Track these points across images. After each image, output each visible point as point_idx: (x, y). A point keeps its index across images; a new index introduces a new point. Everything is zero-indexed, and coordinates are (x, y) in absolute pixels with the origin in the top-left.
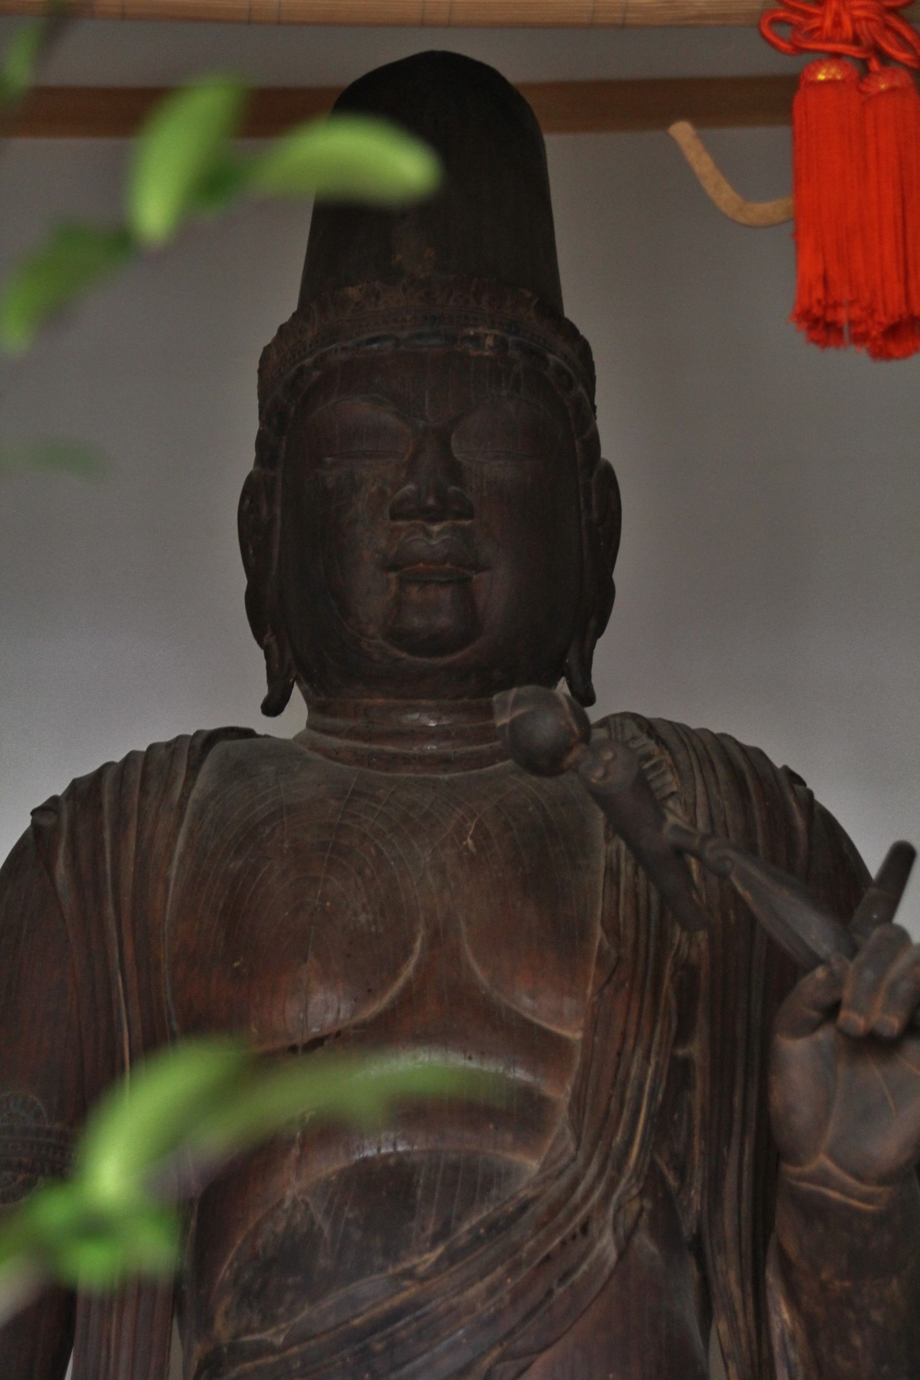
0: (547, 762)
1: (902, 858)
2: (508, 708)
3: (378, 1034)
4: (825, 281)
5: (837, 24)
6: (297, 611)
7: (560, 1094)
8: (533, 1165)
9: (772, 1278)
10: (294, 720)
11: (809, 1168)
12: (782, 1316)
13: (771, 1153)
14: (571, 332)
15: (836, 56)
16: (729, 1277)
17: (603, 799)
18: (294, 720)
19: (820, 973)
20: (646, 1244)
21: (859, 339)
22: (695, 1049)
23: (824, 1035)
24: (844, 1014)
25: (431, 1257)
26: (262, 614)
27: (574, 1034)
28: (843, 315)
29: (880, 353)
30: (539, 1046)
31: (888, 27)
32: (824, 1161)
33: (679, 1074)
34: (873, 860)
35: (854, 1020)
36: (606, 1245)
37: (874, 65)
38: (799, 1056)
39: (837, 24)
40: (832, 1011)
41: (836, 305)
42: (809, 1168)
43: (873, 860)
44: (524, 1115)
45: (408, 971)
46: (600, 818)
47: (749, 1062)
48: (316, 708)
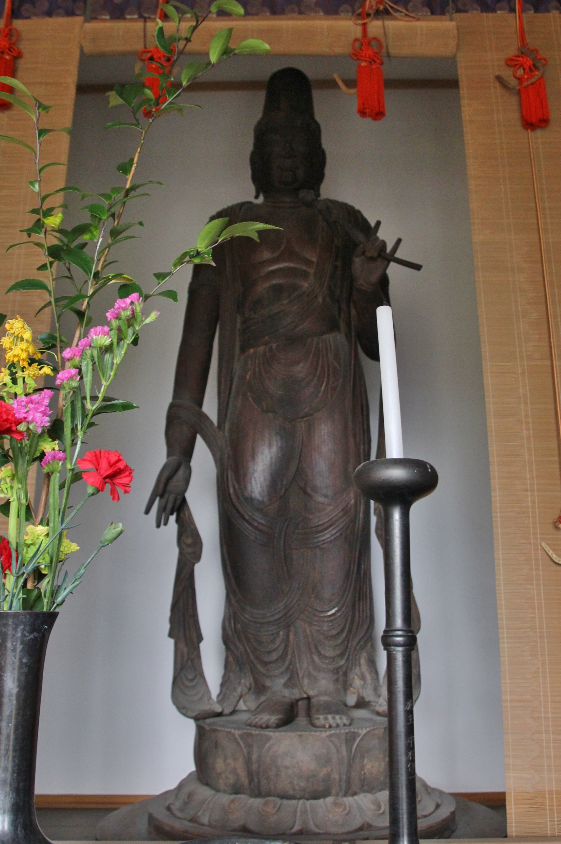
0: (309, 205)
1: (378, 223)
2: (302, 194)
3: (276, 260)
4: (363, 104)
5: (365, 54)
6: (262, 175)
7: (312, 271)
8: (306, 285)
9: (352, 304)
10: (261, 200)
11: (359, 283)
12: (353, 312)
13: (352, 280)
14: (316, 123)
15: (365, 61)
16: (344, 306)
17: (320, 211)
18: (261, 200)
19: (362, 245)
20: (328, 299)
21: (370, 116)
22: (339, 263)
23: (363, 257)
24: (366, 253)
25: (286, 301)
26: (255, 179)
27: (314, 259)
28: (367, 111)
29: (374, 119)
30: (308, 262)
31: (376, 56)
32: (362, 282)
33: (335, 267)
34: (373, 224)
35: (368, 254)
36: (320, 300)
37: (373, 63)
38: (357, 261)
39: (365, 54)
40: (364, 253)
41: (366, 108)
42: (359, 283)
43: (373, 224)
44: (305, 275)
45: (282, 248)
46: (321, 218)
47: (347, 263)
48: (265, 197)
